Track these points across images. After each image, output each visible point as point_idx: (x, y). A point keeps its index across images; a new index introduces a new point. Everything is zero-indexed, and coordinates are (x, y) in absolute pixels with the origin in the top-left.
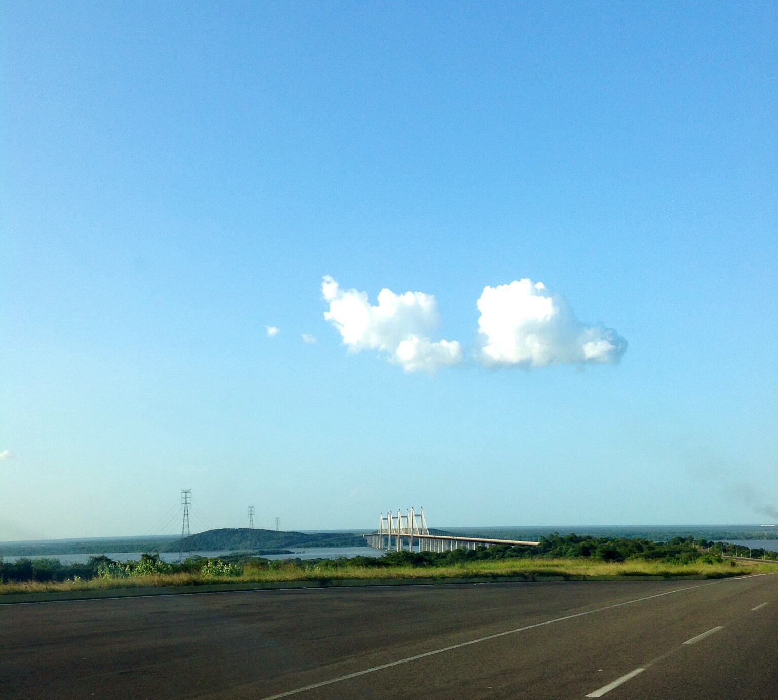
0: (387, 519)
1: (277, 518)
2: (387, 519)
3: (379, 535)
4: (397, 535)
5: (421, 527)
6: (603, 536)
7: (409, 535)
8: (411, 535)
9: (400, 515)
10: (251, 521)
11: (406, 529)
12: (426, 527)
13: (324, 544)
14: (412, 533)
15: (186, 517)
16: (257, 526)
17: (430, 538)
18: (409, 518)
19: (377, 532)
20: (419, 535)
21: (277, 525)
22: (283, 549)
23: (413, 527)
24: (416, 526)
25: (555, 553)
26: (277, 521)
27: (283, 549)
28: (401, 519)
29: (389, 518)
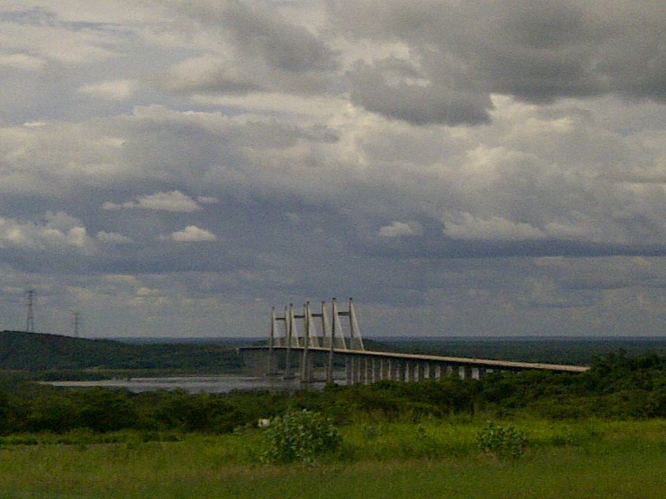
0: (284, 319)
1: (78, 314)
2: (284, 319)
3: (268, 349)
4: (302, 350)
5: (321, 335)
6: (169, 194)
7: (266, 347)
8: (269, 347)
9: (310, 312)
10: (30, 317)
11: (320, 339)
12: (358, 335)
13: (533, 370)
14: (332, 347)
15: (30, 320)
16: (40, 329)
17: (367, 355)
18: (326, 320)
19: (264, 342)
20: (346, 350)
21: (76, 327)
22: (88, 370)
23: (333, 334)
24: (340, 333)
25: (96, 394)
26: (77, 319)
27: (88, 370)
28: (311, 319)
29: (287, 318)
